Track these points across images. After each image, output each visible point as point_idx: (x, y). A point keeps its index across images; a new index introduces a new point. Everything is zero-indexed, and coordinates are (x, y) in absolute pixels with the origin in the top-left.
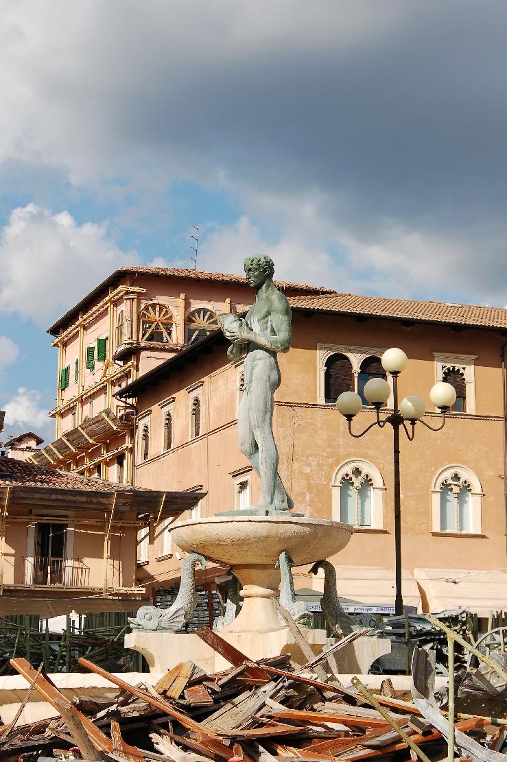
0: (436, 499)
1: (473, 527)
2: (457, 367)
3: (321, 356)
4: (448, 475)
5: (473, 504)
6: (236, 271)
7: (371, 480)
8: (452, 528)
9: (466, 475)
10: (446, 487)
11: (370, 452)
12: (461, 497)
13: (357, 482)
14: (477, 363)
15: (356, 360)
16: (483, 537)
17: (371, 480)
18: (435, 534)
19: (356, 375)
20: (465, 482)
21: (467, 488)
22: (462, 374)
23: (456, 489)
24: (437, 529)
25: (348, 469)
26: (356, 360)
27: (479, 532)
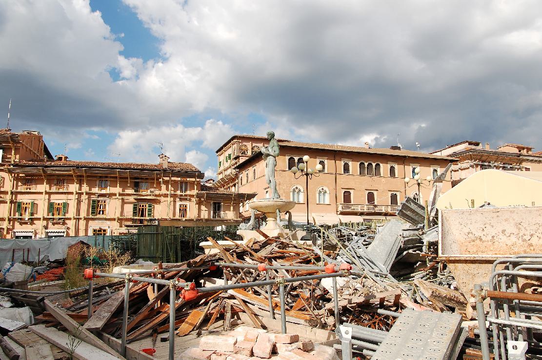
0: (291, 193)
1: (327, 202)
5: (327, 196)
8: (322, 202)
10: (294, 191)
13: (297, 191)
14: (441, 167)
24: (318, 203)
25: (294, 187)
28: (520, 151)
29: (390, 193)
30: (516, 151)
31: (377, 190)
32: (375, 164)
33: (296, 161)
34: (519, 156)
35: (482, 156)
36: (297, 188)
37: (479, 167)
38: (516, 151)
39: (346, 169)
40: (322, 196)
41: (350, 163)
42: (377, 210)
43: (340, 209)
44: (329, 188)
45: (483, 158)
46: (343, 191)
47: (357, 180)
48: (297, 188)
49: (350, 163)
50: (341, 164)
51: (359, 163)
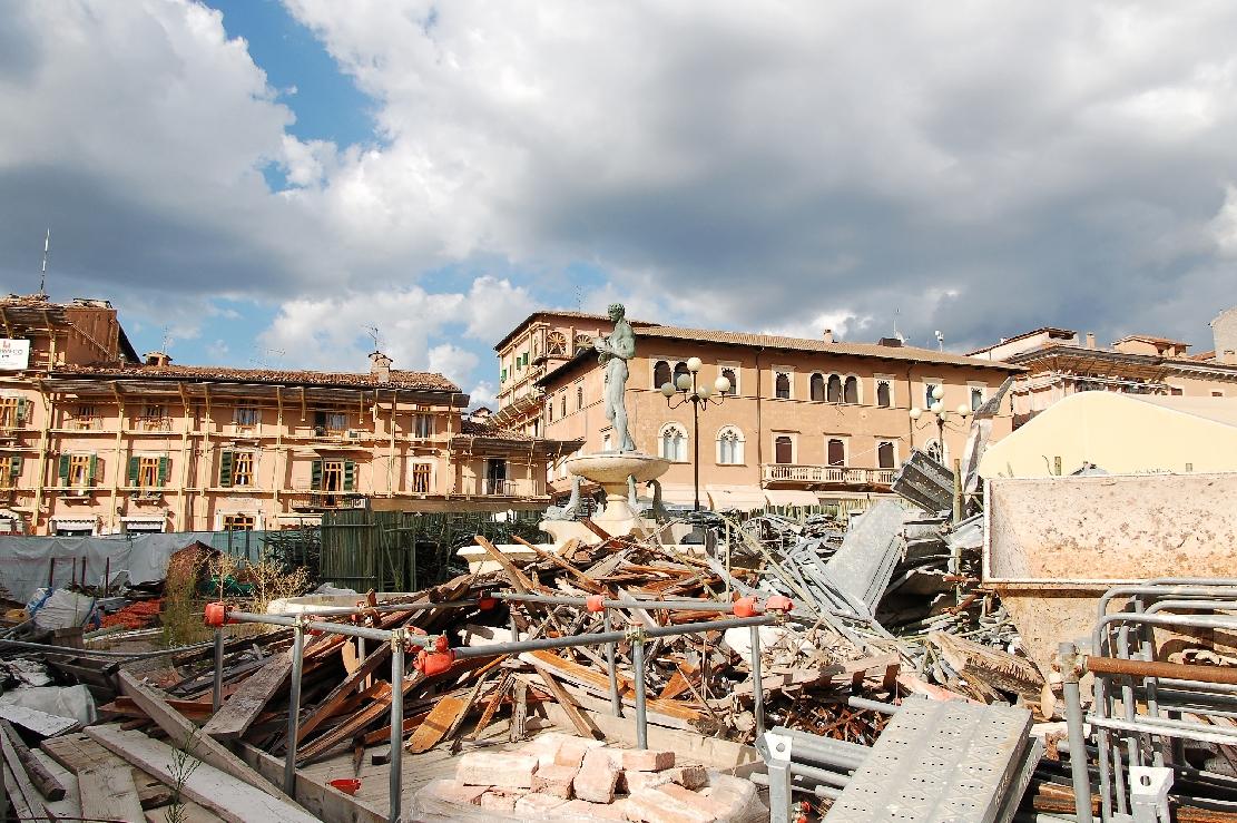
1: (739, 460)
3: (653, 362)
5: (739, 447)
10: (667, 435)
12: (676, 442)
13: (674, 435)
18: (718, 465)
24: (719, 462)
28: (1161, 352)
29: (878, 442)
30: (1152, 351)
33: (843, 382)
34: (1158, 363)
35: (1078, 362)
36: (730, 432)
37: (1073, 385)
38: (1152, 351)
39: (782, 388)
40: (671, 446)
41: (892, 383)
44: (743, 430)
45: (1083, 366)
50: (771, 376)
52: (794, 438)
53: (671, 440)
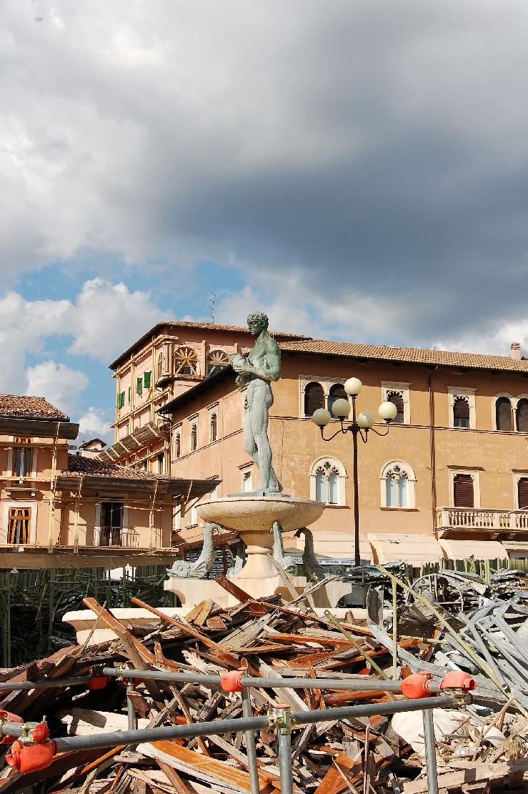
0: (383, 483)
1: (409, 503)
2: (464, 396)
4: (391, 467)
5: (409, 487)
6: (241, 324)
7: (337, 471)
9: (404, 467)
10: (390, 475)
11: (337, 451)
13: (327, 472)
14: (411, 388)
15: (326, 386)
16: (416, 510)
17: (337, 471)
18: (383, 509)
19: (514, 411)
20: (334, 468)
21: (405, 476)
22: (467, 401)
23: (397, 477)
24: (384, 505)
25: (321, 463)
26: (326, 386)
27: (414, 508)
31: (481, 469)
32: (332, 384)
36: (328, 465)
40: (325, 485)
42: (479, 522)
43: (444, 521)
44: (413, 467)
46: (453, 473)
47: (490, 446)
48: (328, 465)
49: (471, 400)
50: (446, 401)
51: (495, 399)
52: (476, 476)
53: (394, 483)
